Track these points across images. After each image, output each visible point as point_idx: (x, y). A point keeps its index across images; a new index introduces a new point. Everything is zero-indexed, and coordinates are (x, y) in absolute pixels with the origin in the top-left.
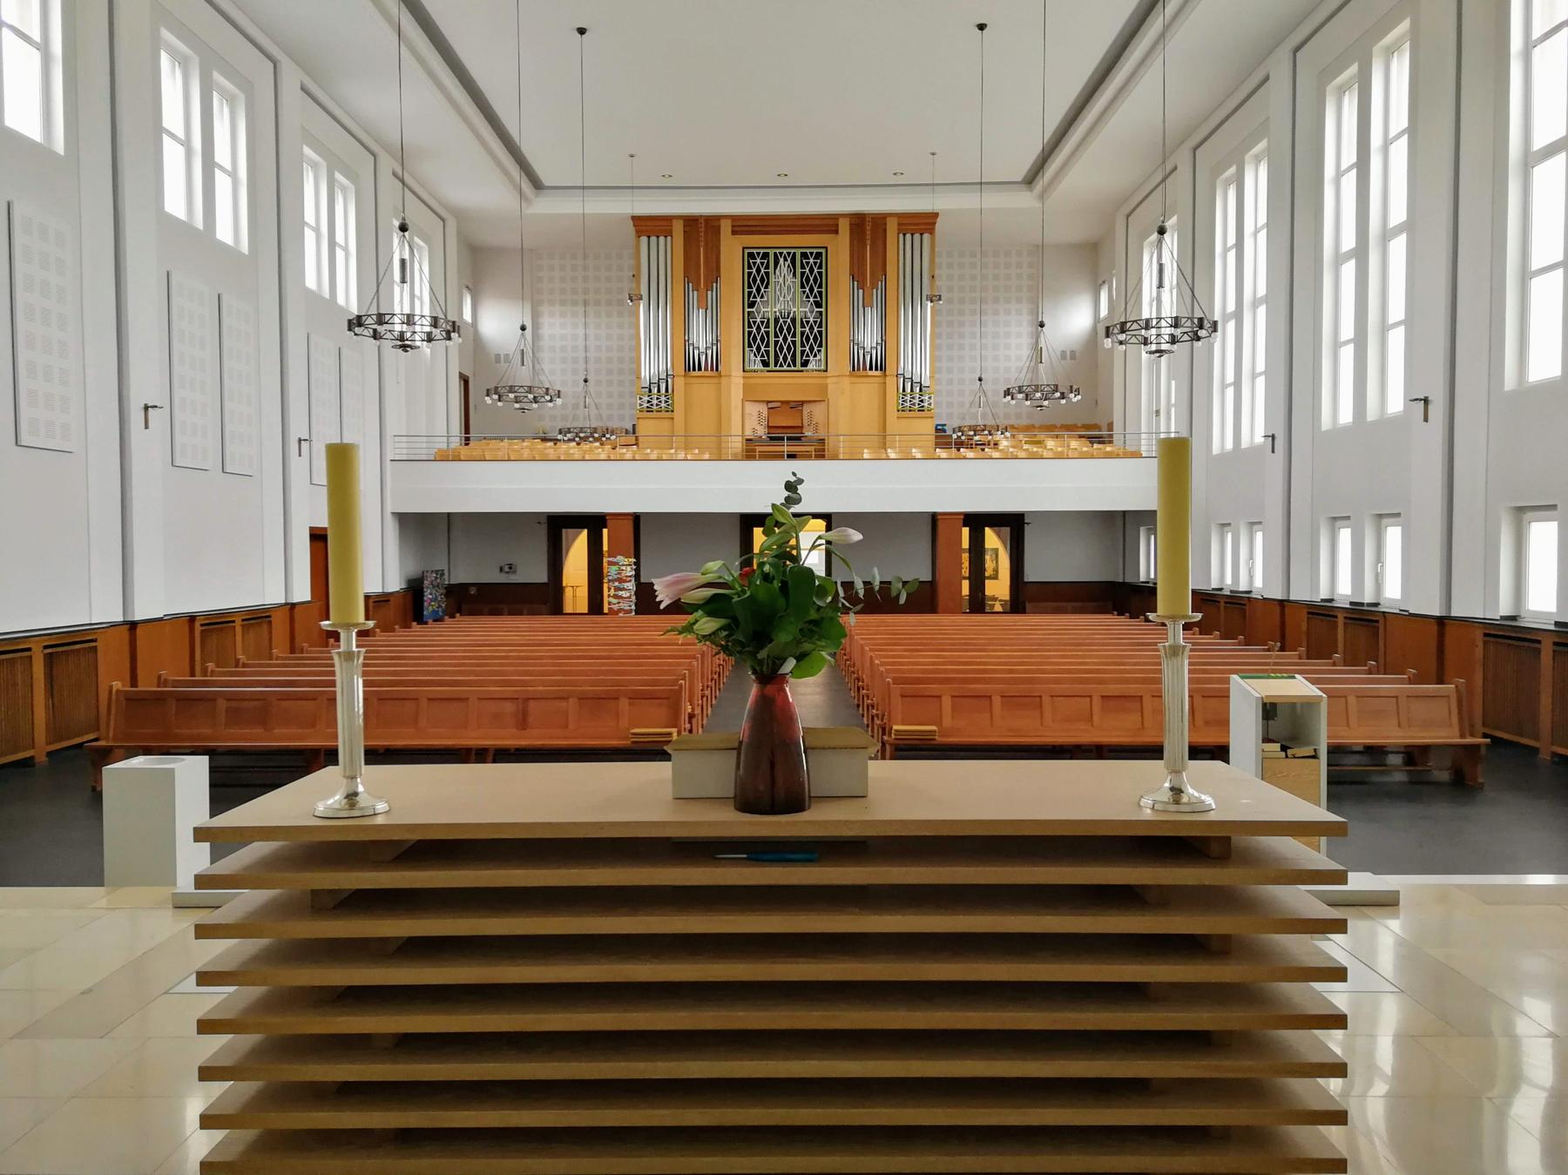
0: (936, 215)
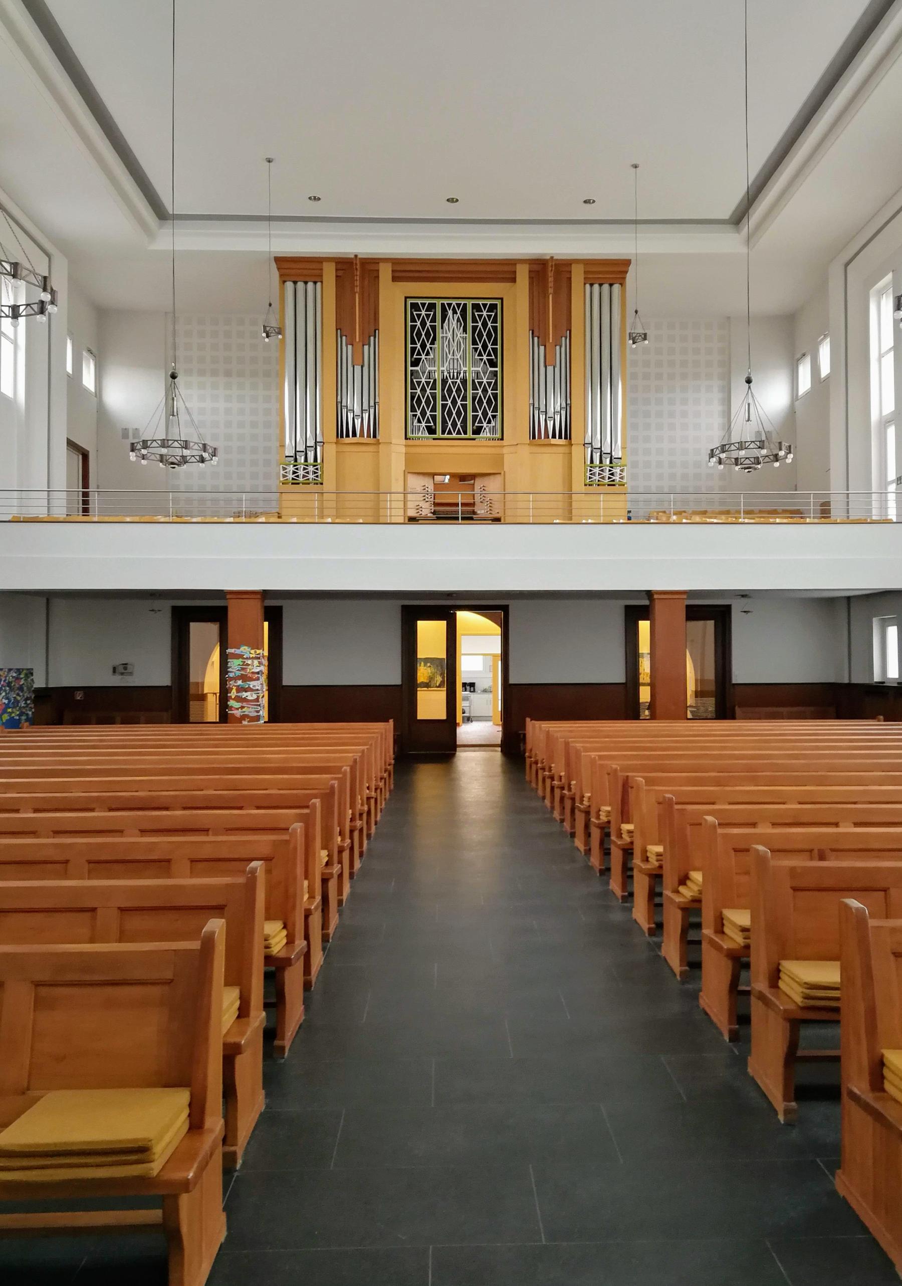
0: (627, 263)
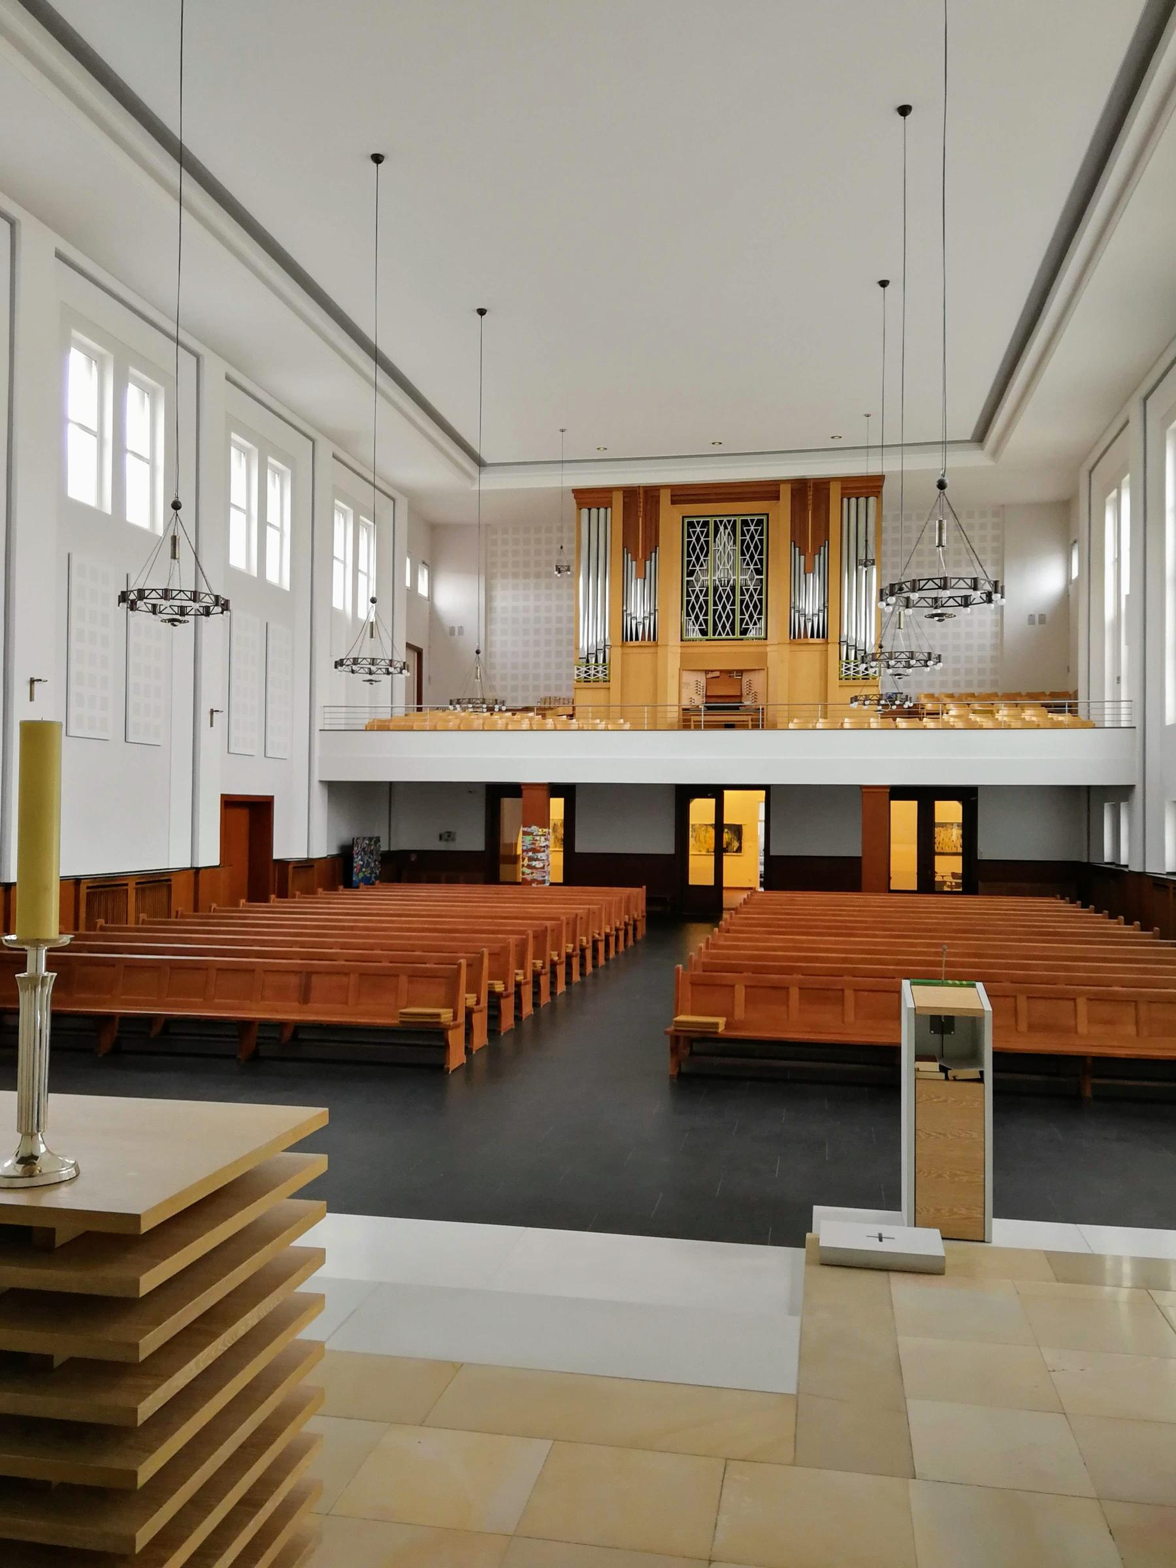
0: (881, 478)
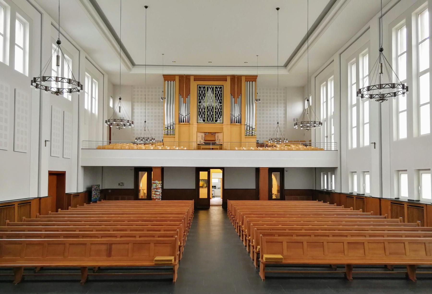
0: (257, 76)
